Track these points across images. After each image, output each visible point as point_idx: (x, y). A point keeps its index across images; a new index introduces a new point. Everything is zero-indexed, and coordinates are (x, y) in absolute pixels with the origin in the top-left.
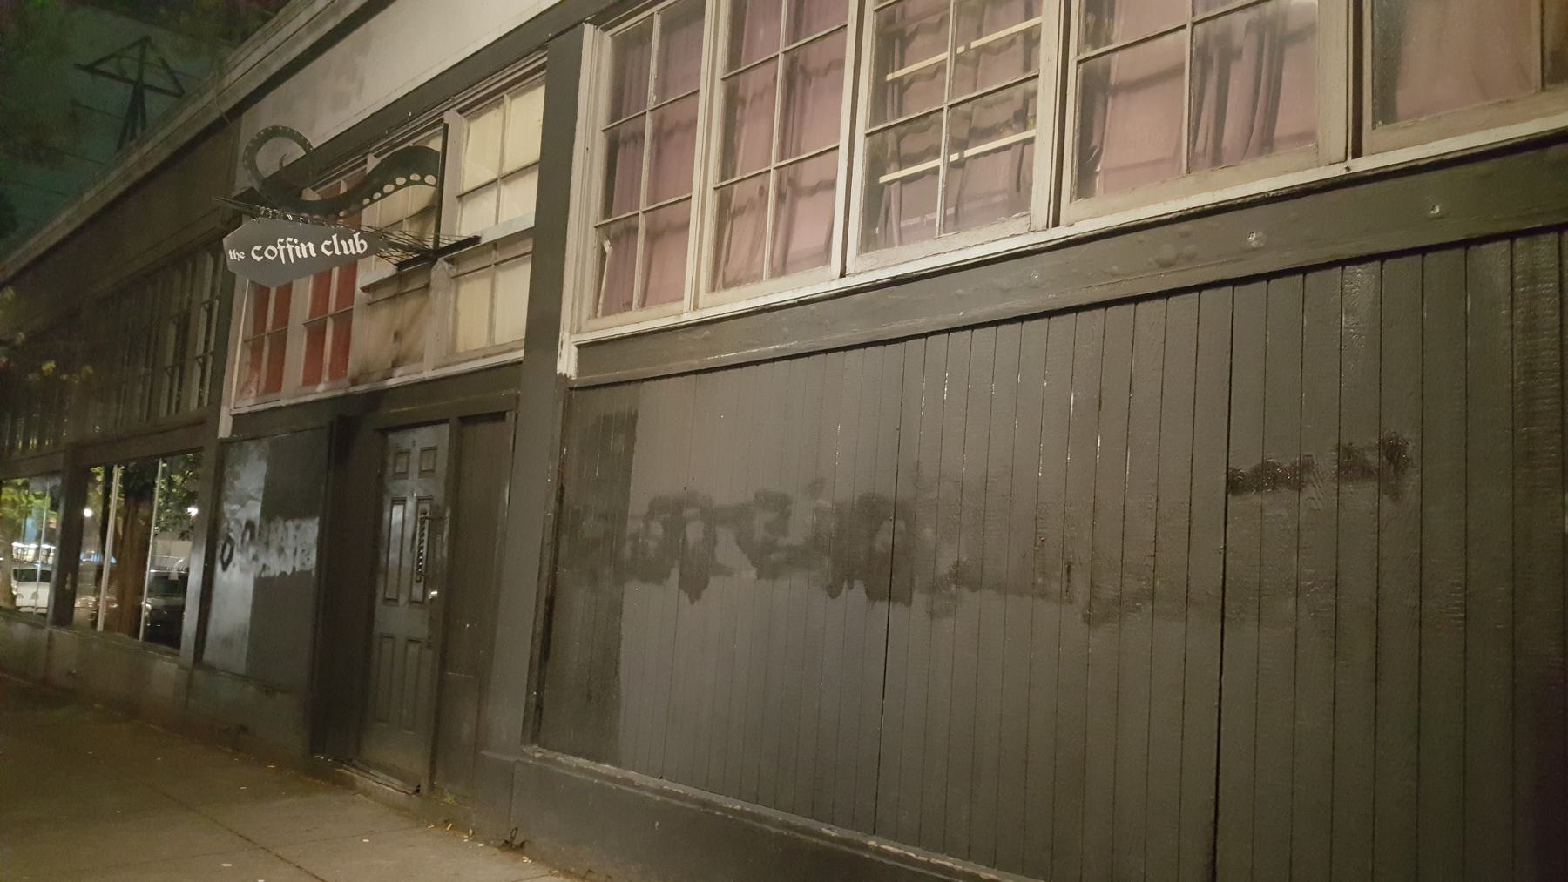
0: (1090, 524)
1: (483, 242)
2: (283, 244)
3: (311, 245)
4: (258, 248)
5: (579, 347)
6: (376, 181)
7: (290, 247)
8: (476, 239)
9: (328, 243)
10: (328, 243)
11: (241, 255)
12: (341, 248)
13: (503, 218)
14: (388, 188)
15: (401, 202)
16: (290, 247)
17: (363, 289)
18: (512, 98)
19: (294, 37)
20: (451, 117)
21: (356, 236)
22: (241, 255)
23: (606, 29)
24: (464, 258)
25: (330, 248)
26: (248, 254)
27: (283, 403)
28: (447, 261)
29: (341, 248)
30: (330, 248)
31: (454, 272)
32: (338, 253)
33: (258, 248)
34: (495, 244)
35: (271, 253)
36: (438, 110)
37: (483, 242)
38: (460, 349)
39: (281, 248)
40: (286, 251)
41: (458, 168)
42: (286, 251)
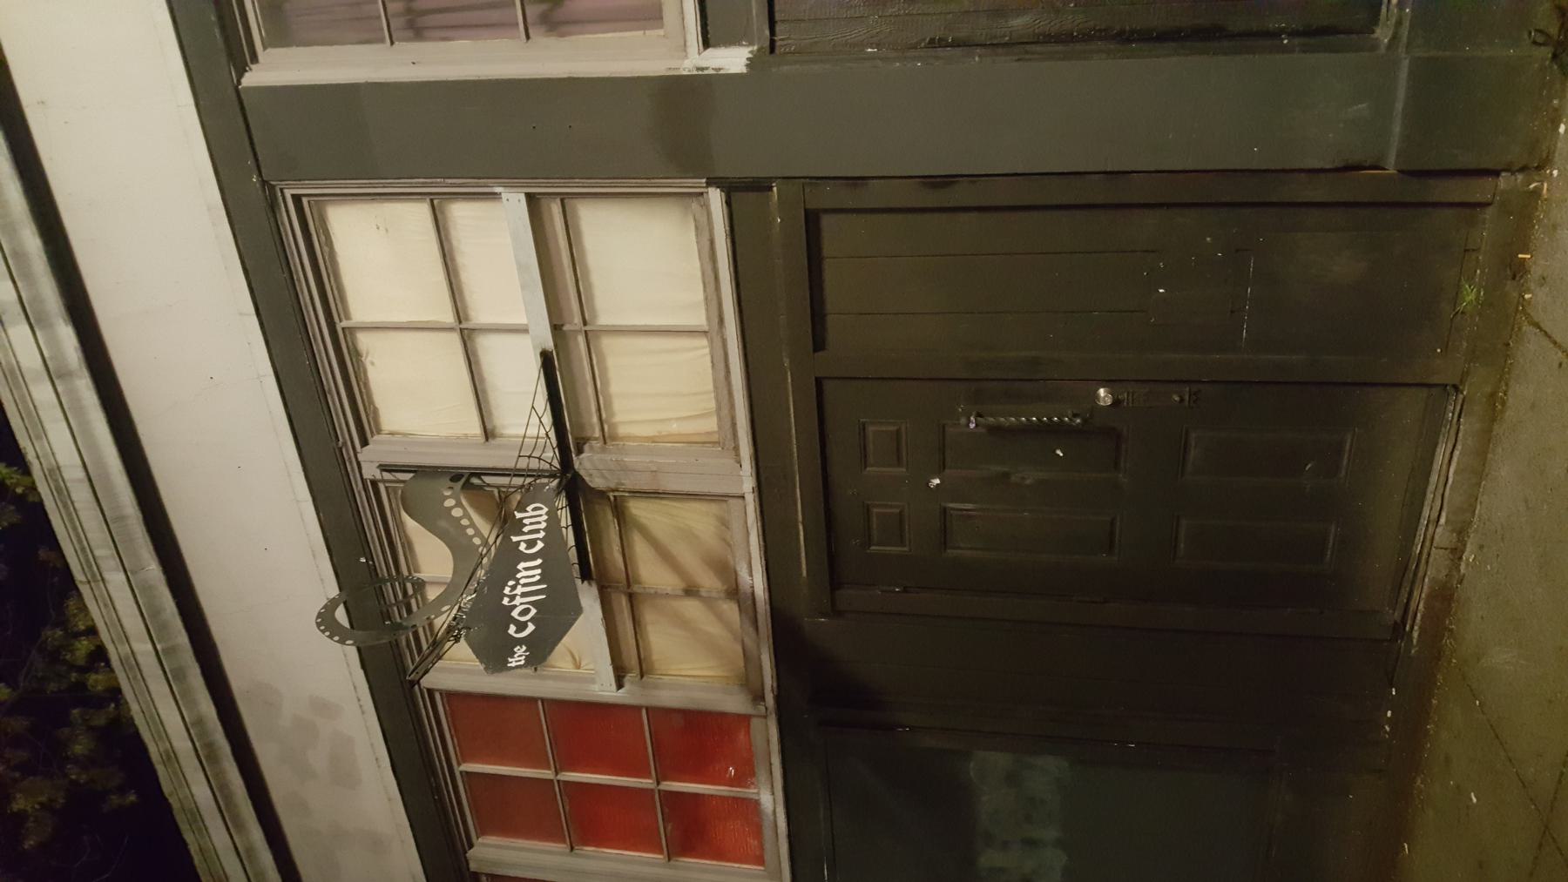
0: (963, 33)
2: (512, 598)
3: (521, 566)
4: (512, 629)
5: (706, 44)
6: (443, 524)
7: (519, 590)
8: (547, 360)
9: (522, 547)
11: (520, 651)
13: (520, 319)
17: (620, 686)
18: (348, 317)
19: (193, 727)
21: (518, 515)
22: (520, 651)
23: (255, 59)
24: (579, 426)
25: (531, 544)
26: (520, 642)
28: (580, 451)
30: (531, 544)
31: (597, 445)
32: (542, 534)
33: (512, 629)
34: (556, 328)
35: (525, 612)
36: (358, 487)
37: (549, 345)
39: (518, 601)
40: (524, 595)
41: (447, 442)
42: (524, 595)
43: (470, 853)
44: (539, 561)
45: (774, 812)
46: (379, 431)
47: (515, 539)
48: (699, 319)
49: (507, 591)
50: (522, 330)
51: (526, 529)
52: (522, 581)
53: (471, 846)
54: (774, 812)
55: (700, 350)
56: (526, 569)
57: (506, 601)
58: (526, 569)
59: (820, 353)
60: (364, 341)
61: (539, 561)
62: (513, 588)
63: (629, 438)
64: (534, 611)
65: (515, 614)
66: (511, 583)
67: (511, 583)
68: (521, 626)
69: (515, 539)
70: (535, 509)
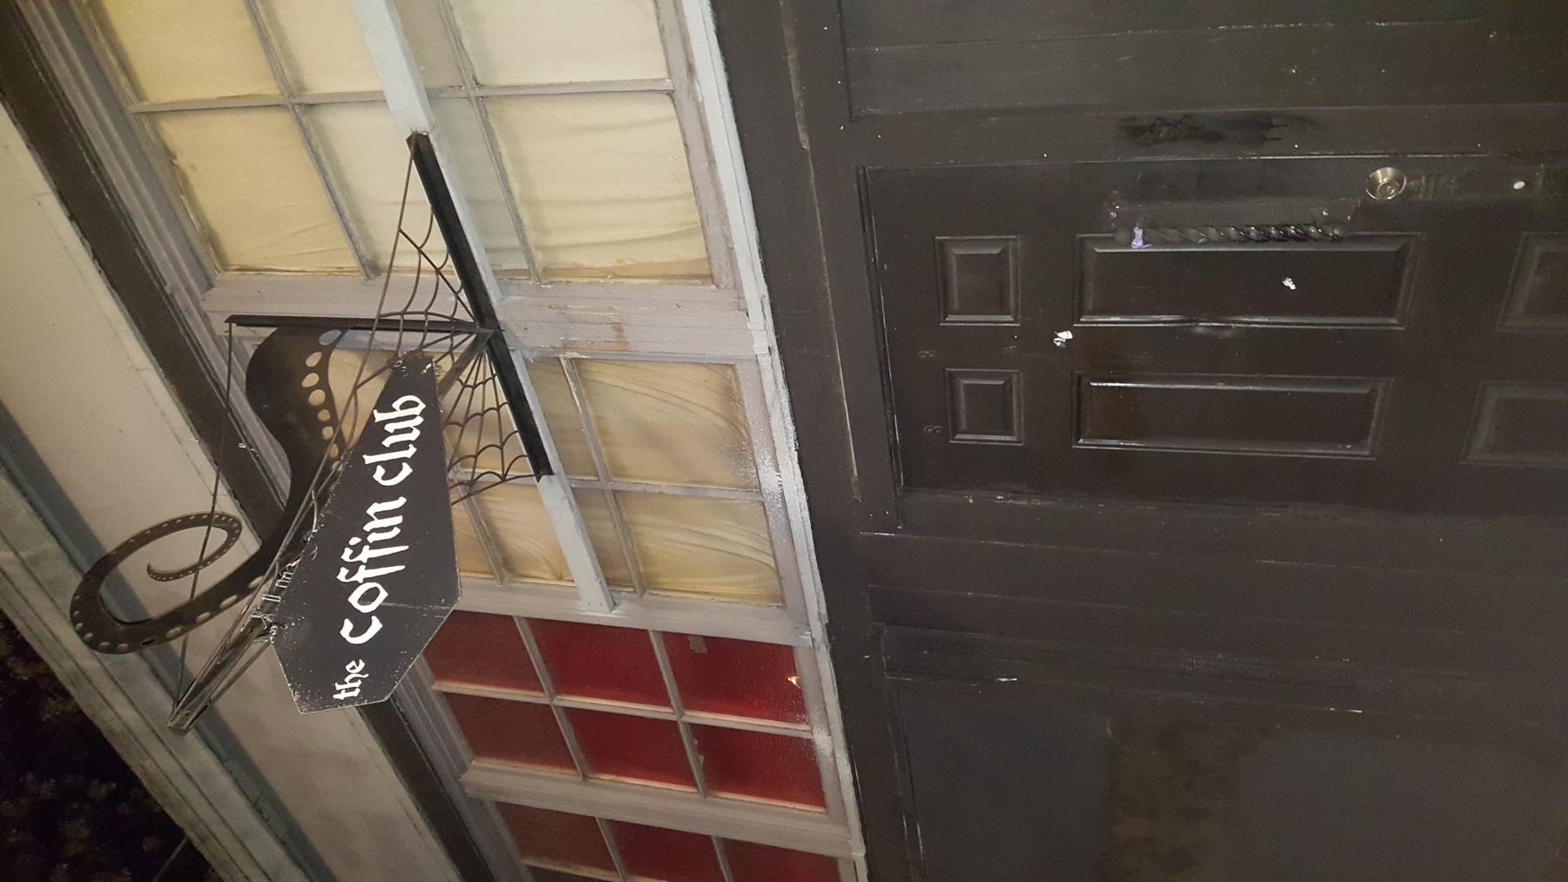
1: (422, 124)
2: (353, 569)
4: (348, 626)
7: (367, 554)
8: (422, 152)
9: (379, 473)
10: (379, 473)
11: (355, 669)
12: (403, 446)
14: (317, 397)
15: (344, 380)
16: (367, 554)
18: (140, 95)
20: (134, 108)
22: (355, 669)
25: (392, 468)
27: (859, 854)
29: (403, 446)
30: (392, 468)
33: (348, 626)
35: (369, 596)
38: (690, 251)
39: (362, 573)
40: (373, 563)
42: (373, 563)
43: (464, 777)
44: (402, 501)
45: (833, 754)
46: (225, 266)
47: (369, 459)
48: (650, 66)
49: (347, 555)
50: (375, 100)
51: (387, 442)
52: (372, 538)
53: (464, 769)
54: (833, 754)
55: (656, 130)
56: (381, 515)
57: (342, 575)
58: (381, 515)
59: (389, 96)
60: (176, 133)
61: (402, 501)
62: (357, 550)
63: (576, 270)
64: (383, 594)
65: (354, 599)
66: (354, 541)
67: (354, 541)
68: (362, 623)
69: (369, 459)
70: (405, 406)
